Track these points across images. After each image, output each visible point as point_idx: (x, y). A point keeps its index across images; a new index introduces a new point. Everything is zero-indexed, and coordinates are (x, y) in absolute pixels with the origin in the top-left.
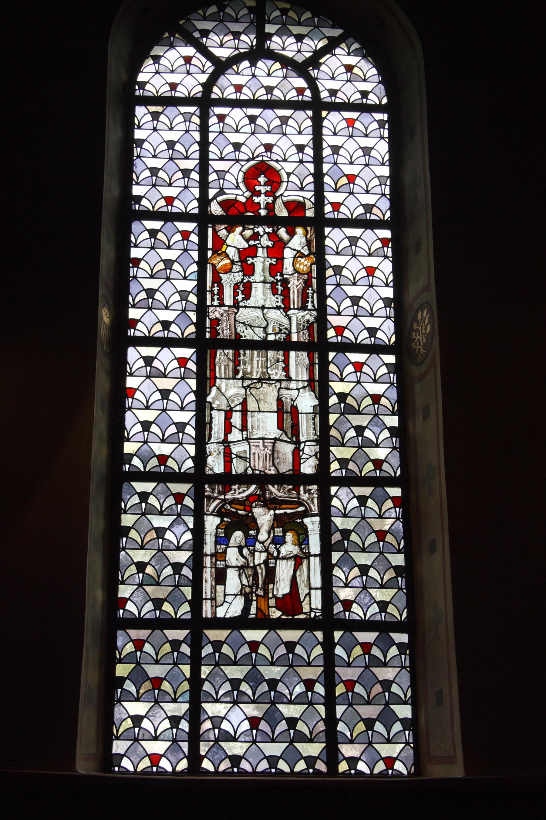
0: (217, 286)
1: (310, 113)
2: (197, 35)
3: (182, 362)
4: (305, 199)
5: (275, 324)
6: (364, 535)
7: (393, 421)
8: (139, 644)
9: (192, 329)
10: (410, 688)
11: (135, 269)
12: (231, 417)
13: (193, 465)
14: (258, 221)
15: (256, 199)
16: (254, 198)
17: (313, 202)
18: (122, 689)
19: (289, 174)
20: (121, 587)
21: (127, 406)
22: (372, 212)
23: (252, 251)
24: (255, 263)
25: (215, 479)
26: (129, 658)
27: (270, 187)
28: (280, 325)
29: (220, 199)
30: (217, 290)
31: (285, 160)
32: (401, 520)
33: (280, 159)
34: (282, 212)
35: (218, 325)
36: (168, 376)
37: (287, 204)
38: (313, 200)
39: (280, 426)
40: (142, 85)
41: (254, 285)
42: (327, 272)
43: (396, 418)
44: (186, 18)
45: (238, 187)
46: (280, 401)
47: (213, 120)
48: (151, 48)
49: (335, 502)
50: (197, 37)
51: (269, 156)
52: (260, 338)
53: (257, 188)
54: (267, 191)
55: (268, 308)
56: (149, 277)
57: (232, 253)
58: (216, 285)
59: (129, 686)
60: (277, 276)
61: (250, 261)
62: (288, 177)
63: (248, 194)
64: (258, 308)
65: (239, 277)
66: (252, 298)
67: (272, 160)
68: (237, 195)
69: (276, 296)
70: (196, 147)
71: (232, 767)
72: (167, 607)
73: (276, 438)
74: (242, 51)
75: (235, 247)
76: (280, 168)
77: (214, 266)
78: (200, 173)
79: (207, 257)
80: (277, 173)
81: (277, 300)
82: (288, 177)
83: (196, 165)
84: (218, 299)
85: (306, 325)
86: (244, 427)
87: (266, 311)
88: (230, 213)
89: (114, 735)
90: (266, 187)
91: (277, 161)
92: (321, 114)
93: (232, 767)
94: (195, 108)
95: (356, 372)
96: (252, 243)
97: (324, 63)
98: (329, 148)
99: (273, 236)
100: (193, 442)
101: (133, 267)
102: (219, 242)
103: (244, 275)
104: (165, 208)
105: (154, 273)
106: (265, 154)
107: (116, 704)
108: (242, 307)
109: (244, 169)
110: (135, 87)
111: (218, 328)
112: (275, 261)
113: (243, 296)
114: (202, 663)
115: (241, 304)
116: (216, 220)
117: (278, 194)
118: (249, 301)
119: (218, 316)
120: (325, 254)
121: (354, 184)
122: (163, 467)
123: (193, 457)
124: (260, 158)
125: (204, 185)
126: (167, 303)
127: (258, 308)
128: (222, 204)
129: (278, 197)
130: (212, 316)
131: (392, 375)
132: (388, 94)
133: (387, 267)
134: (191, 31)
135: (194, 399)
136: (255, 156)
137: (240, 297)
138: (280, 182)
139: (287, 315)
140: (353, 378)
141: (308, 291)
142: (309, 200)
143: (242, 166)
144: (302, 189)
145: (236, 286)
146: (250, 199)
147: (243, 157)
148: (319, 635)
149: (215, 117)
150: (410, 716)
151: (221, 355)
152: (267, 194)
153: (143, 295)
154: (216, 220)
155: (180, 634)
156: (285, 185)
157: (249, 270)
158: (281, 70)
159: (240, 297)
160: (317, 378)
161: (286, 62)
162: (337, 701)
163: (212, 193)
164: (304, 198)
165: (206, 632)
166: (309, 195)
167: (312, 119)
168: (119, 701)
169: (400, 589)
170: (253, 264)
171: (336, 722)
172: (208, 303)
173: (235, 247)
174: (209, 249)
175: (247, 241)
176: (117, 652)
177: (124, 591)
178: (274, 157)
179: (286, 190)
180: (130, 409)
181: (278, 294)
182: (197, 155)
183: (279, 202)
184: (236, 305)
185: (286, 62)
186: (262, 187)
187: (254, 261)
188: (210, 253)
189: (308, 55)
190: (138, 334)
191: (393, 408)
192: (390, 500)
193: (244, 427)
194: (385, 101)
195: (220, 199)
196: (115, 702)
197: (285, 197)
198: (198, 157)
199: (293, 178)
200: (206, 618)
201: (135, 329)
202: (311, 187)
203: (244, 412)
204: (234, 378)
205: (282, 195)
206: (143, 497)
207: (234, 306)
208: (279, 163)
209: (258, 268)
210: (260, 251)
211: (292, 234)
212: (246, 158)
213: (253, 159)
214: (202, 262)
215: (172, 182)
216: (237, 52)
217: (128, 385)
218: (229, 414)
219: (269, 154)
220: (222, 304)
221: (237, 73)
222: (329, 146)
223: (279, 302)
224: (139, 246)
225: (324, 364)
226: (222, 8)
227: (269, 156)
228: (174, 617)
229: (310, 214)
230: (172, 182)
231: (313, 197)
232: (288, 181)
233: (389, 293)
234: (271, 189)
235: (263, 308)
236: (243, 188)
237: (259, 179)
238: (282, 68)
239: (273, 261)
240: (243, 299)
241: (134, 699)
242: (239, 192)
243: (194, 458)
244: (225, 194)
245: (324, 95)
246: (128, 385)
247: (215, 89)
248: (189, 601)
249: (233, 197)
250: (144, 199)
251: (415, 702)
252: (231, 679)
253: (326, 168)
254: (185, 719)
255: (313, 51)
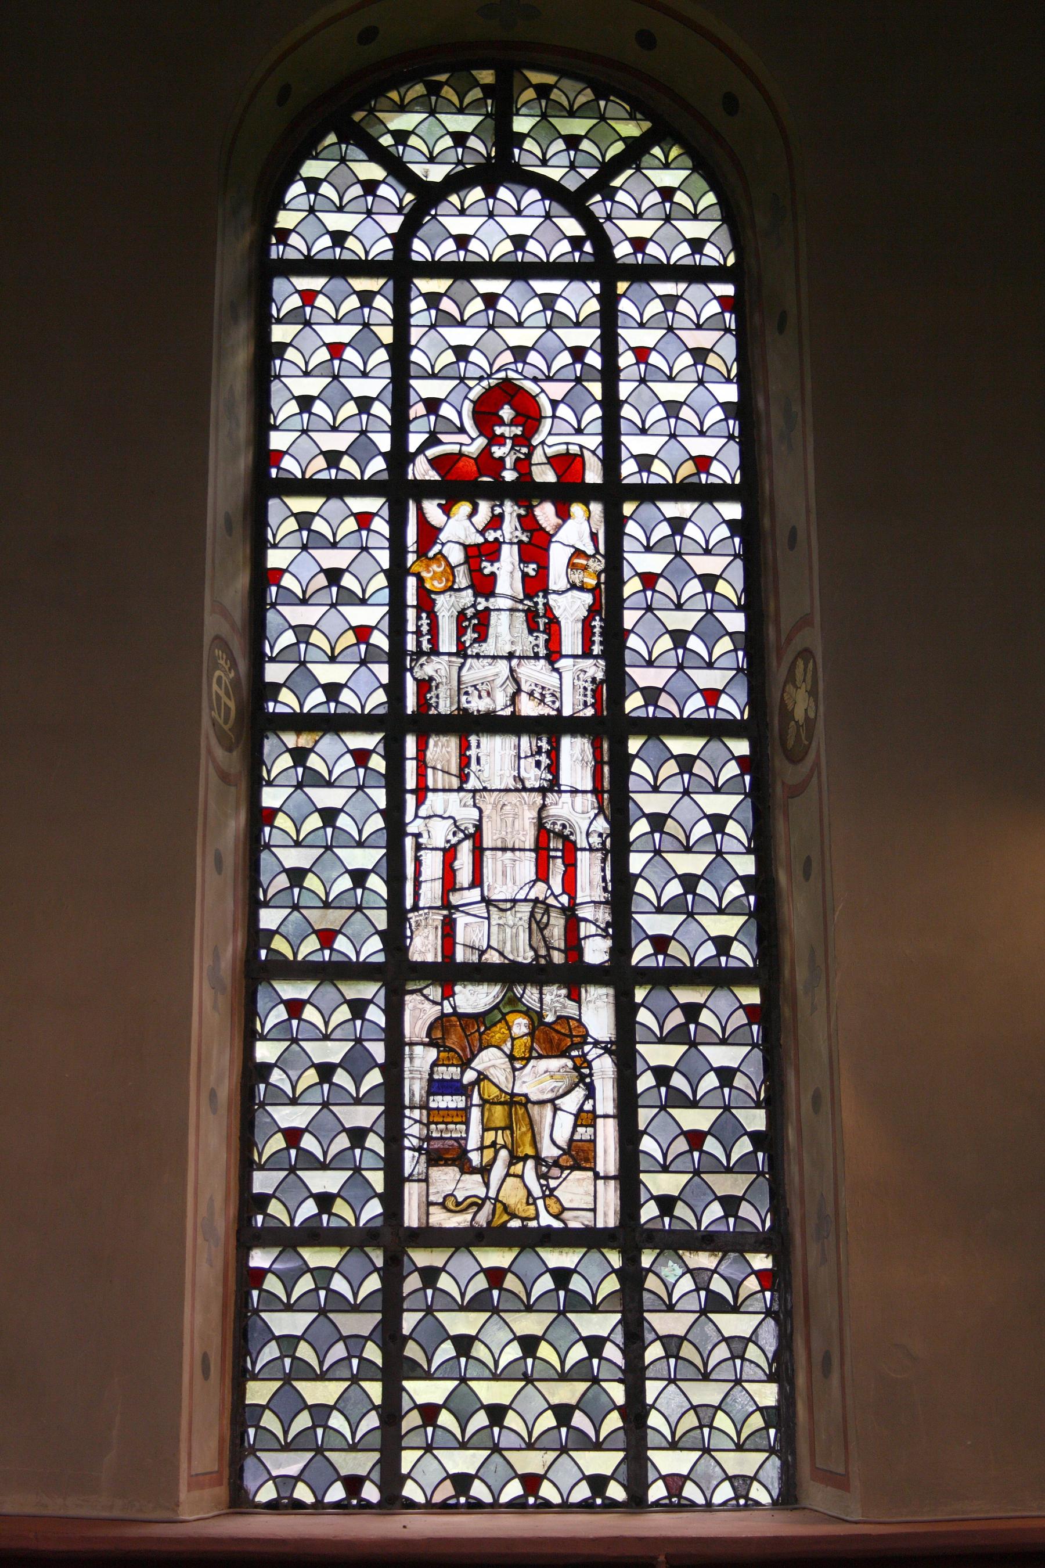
0: (427, 618)
1: (596, 287)
2: (387, 141)
3: (361, 757)
4: (585, 451)
5: (533, 687)
6: (708, 1489)
7: (756, 1120)
8: (308, 297)
9: (374, 1208)
10: (769, 1214)
11: (281, 248)
12: (455, 858)
13: (384, 466)
14: (498, 492)
15: (498, 452)
16: (494, 449)
17: (601, 456)
18: (268, 1084)
19: (555, 404)
20: (273, 435)
21: (273, 374)
22: (707, 363)
23: (492, 551)
24: (497, 572)
25: (426, 972)
26: (295, 317)
27: (521, 428)
28: (543, 688)
29: (432, 452)
30: (428, 624)
31: (549, 379)
32: (767, 1176)
33: (541, 376)
34: (545, 475)
35: (430, 690)
36: (332, 1037)
37: (553, 461)
38: (600, 452)
39: (542, 875)
40: (283, 235)
41: (494, 615)
42: (643, 1211)
43: (762, 1113)
44: (367, 107)
45: (462, 430)
46: (543, 832)
47: (417, 305)
48: (300, 164)
49: (651, 1282)
50: (385, 144)
51: (520, 371)
52: (504, 538)
53: (498, 430)
54: (516, 435)
55: (520, 658)
56: (293, 844)
57: (456, 555)
58: (424, 615)
59: (270, 1421)
60: (538, 596)
61: (488, 568)
62: (554, 409)
63: (482, 442)
64: (502, 657)
65: (467, 597)
66: (491, 640)
67: (526, 378)
68: (461, 444)
69: (535, 634)
70: (381, 581)
71: (457, 1496)
72: (347, 463)
73: (537, 898)
74: (468, 166)
75: (460, 544)
76: (537, 390)
77: (420, 580)
78: (390, 522)
79: (402, 1293)
80: (532, 400)
81: (537, 642)
82: (554, 409)
83: (374, 1466)
84: (429, 641)
85: (590, 686)
86: (477, 880)
87: (514, 662)
88: (449, 477)
89: (264, 779)
90: (513, 428)
91: (535, 380)
92: (616, 287)
93: (457, 1496)
94: (380, 501)
95: (681, 773)
96: (491, 536)
97: (620, 188)
98: (632, 460)
99: (529, 522)
100: (387, 544)
101: (277, 244)
102: (429, 534)
103: (476, 595)
104: (327, 472)
105: (298, 1092)
106: (513, 366)
107: (251, 1316)
108: (472, 656)
109: (474, 395)
110: (270, 239)
111: (428, 696)
112: (534, 569)
113: (476, 635)
114: (405, 1307)
115: (469, 652)
116: (423, 490)
117: (535, 442)
118: (484, 645)
119: (431, 673)
120: (616, 326)
121: (683, 536)
122: (332, 705)
123: (381, 1194)
124: (502, 375)
125: (400, 428)
126: (333, 649)
127: (502, 657)
128: (435, 463)
129: (535, 447)
130: (419, 674)
131: (731, 422)
132: (737, 246)
133: (728, 347)
134: (374, 134)
135: (384, 699)
136: (493, 372)
137: (469, 636)
138: (539, 418)
139: (557, 670)
140: (664, 427)
141: (593, 624)
142: (593, 452)
143: (470, 389)
144: (579, 431)
145: (461, 616)
146: (486, 451)
147: (473, 372)
148: (616, 1259)
149: (421, 299)
150: (747, 753)
151: (436, 745)
152: (516, 440)
153: (288, 638)
154: (423, 490)
155: (368, 990)
156: (548, 422)
157: (484, 586)
158: (541, 202)
159: (469, 636)
160: (606, 759)
161: (550, 190)
162: (621, 374)
163: (414, 441)
164: (581, 447)
165: (417, 281)
166: (593, 441)
167: (599, 297)
168: (273, 605)
169: (727, 330)
170: (493, 575)
171: (620, 404)
172: (409, 903)
173: (460, 544)
174: (412, 791)
175: (482, 533)
176: (264, 768)
177: (277, 441)
178: (529, 371)
179: (550, 434)
180: (278, 377)
181: (538, 631)
182: (385, 596)
183: (538, 456)
184: (462, 652)
185: (550, 190)
186: (508, 428)
187: (494, 569)
188: (411, 558)
189: (589, 173)
190: (280, 709)
191: (758, 1094)
192: (745, 1138)
193: (477, 880)
194: (731, 260)
195: (432, 452)
196: (256, 1107)
197: (549, 446)
198: (387, 601)
199: (563, 411)
200: (409, 1228)
201: (276, 701)
202: (597, 427)
203: (478, 852)
204: (460, 789)
205: (543, 443)
206: (295, 1007)
207: (456, 654)
208: (539, 383)
209: (502, 586)
210: (505, 549)
211: (564, 515)
212: (479, 373)
213: (489, 377)
214: (396, 575)
215: (344, 204)
216: (460, 168)
217: (273, 446)
218: (450, 854)
219: (520, 366)
220: (435, 651)
221: (462, 212)
222: (633, 456)
223: (541, 646)
224: (280, 546)
225: (621, 764)
226: (434, 89)
227: (520, 371)
228: (354, 1224)
229: (593, 475)
230: (344, 203)
231: (601, 447)
232: (554, 417)
233: (729, 393)
234: (523, 431)
235: (510, 656)
236: (473, 432)
237: (501, 413)
238: (543, 199)
239: (531, 569)
240: (475, 641)
241: (282, 1307)
242: (463, 438)
243: (380, 1410)
244: (440, 443)
245: (622, 250)
246: (273, 446)
247: (417, 245)
248: (381, 1066)
249: (455, 449)
250: (287, 575)
251: (743, 381)
252: (455, 1475)
253: (625, 389)
254: (378, 754)
255: (599, 165)
